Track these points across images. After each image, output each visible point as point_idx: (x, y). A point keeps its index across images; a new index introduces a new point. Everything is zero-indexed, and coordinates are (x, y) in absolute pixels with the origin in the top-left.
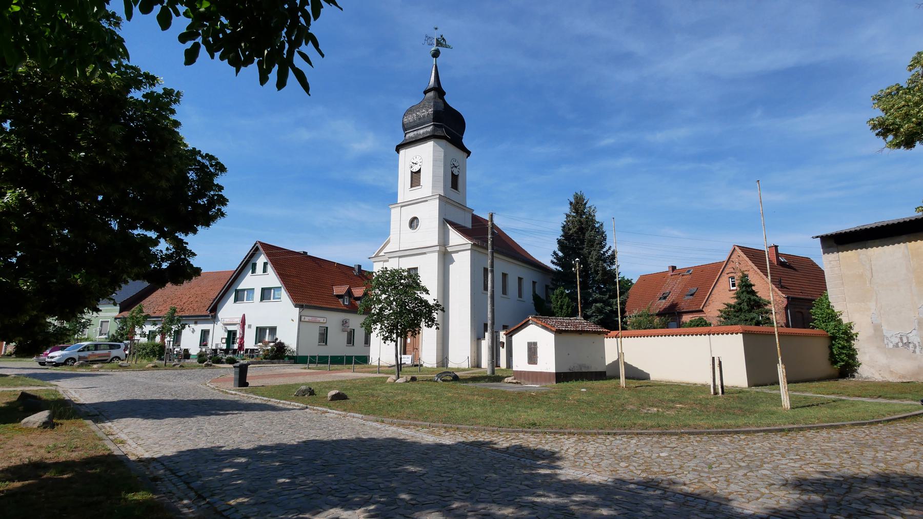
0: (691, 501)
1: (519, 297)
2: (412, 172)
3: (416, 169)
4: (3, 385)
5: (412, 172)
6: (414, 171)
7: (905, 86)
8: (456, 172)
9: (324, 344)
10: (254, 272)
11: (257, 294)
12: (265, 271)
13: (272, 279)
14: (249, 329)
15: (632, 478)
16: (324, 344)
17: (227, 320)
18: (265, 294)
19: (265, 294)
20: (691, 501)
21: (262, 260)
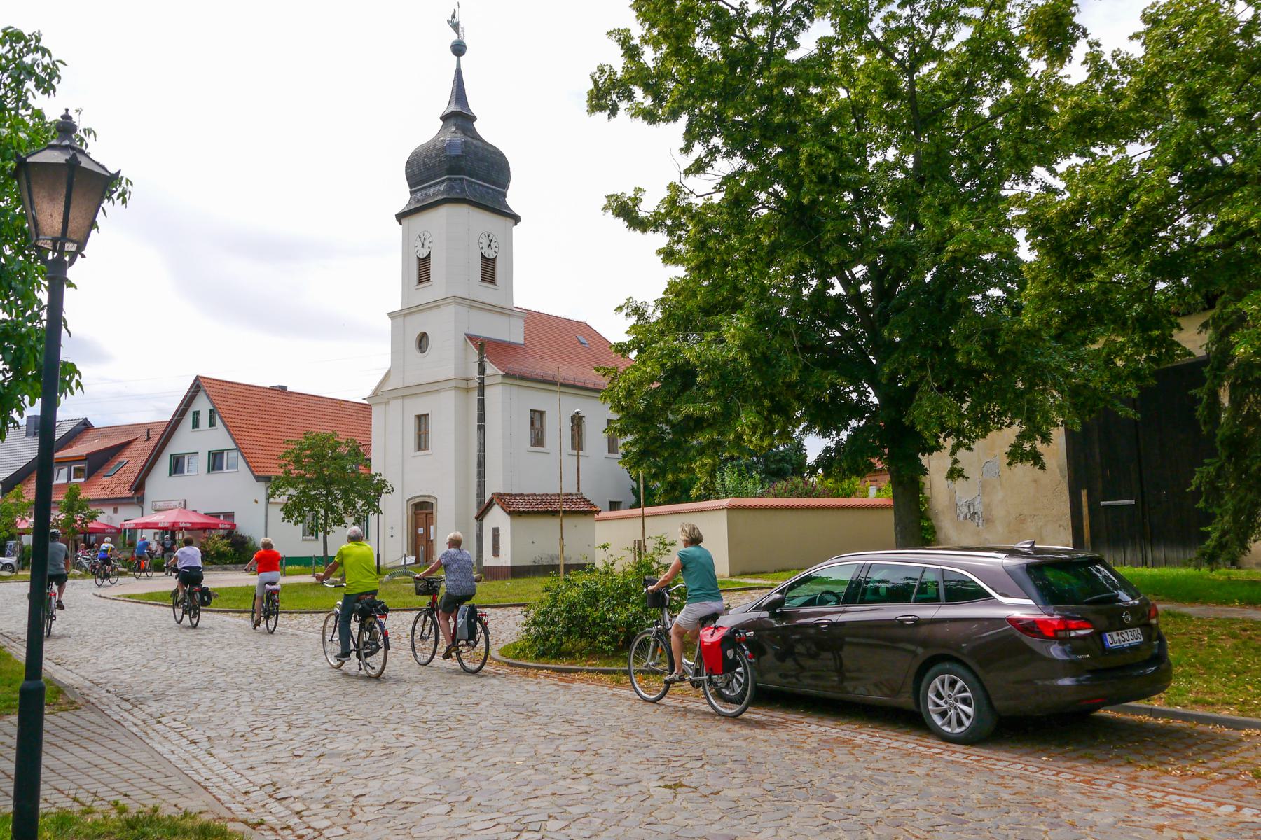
0: (328, 827)
1: (610, 452)
2: (419, 259)
3: (423, 254)
4: (1257, 625)
5: (419, 259)
6: (421, 257)
7: (644, 32)
8: (490, 254)
9: (314, 538)
10: (196, 425)
11: (203, 460)
12: (212, 424)
13: (219, 439)
14: (496, 526)
15: (986, 763)
16: (314, 538)
17: (161, 504)
18: (216, 461)
19: (216, 461)
20: (328, 827)
21: (202, 405)
